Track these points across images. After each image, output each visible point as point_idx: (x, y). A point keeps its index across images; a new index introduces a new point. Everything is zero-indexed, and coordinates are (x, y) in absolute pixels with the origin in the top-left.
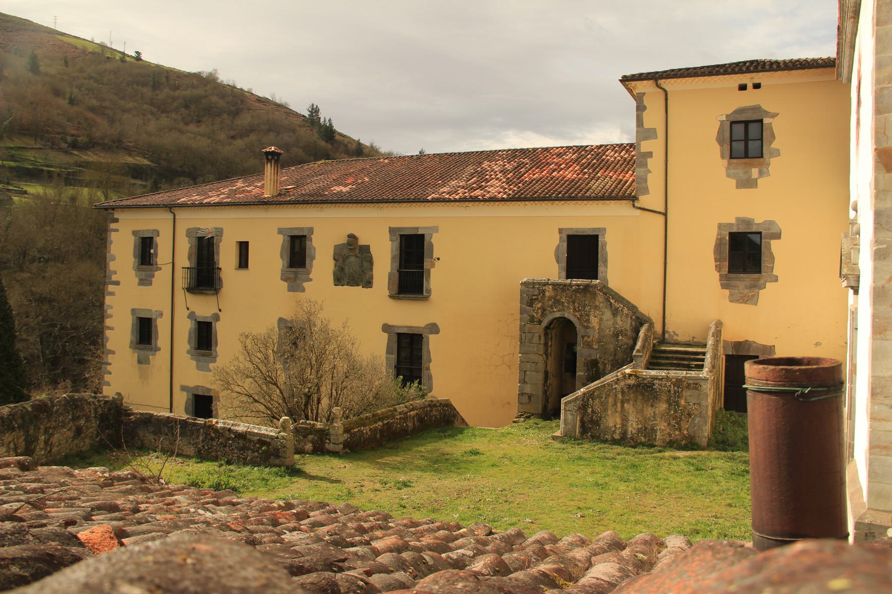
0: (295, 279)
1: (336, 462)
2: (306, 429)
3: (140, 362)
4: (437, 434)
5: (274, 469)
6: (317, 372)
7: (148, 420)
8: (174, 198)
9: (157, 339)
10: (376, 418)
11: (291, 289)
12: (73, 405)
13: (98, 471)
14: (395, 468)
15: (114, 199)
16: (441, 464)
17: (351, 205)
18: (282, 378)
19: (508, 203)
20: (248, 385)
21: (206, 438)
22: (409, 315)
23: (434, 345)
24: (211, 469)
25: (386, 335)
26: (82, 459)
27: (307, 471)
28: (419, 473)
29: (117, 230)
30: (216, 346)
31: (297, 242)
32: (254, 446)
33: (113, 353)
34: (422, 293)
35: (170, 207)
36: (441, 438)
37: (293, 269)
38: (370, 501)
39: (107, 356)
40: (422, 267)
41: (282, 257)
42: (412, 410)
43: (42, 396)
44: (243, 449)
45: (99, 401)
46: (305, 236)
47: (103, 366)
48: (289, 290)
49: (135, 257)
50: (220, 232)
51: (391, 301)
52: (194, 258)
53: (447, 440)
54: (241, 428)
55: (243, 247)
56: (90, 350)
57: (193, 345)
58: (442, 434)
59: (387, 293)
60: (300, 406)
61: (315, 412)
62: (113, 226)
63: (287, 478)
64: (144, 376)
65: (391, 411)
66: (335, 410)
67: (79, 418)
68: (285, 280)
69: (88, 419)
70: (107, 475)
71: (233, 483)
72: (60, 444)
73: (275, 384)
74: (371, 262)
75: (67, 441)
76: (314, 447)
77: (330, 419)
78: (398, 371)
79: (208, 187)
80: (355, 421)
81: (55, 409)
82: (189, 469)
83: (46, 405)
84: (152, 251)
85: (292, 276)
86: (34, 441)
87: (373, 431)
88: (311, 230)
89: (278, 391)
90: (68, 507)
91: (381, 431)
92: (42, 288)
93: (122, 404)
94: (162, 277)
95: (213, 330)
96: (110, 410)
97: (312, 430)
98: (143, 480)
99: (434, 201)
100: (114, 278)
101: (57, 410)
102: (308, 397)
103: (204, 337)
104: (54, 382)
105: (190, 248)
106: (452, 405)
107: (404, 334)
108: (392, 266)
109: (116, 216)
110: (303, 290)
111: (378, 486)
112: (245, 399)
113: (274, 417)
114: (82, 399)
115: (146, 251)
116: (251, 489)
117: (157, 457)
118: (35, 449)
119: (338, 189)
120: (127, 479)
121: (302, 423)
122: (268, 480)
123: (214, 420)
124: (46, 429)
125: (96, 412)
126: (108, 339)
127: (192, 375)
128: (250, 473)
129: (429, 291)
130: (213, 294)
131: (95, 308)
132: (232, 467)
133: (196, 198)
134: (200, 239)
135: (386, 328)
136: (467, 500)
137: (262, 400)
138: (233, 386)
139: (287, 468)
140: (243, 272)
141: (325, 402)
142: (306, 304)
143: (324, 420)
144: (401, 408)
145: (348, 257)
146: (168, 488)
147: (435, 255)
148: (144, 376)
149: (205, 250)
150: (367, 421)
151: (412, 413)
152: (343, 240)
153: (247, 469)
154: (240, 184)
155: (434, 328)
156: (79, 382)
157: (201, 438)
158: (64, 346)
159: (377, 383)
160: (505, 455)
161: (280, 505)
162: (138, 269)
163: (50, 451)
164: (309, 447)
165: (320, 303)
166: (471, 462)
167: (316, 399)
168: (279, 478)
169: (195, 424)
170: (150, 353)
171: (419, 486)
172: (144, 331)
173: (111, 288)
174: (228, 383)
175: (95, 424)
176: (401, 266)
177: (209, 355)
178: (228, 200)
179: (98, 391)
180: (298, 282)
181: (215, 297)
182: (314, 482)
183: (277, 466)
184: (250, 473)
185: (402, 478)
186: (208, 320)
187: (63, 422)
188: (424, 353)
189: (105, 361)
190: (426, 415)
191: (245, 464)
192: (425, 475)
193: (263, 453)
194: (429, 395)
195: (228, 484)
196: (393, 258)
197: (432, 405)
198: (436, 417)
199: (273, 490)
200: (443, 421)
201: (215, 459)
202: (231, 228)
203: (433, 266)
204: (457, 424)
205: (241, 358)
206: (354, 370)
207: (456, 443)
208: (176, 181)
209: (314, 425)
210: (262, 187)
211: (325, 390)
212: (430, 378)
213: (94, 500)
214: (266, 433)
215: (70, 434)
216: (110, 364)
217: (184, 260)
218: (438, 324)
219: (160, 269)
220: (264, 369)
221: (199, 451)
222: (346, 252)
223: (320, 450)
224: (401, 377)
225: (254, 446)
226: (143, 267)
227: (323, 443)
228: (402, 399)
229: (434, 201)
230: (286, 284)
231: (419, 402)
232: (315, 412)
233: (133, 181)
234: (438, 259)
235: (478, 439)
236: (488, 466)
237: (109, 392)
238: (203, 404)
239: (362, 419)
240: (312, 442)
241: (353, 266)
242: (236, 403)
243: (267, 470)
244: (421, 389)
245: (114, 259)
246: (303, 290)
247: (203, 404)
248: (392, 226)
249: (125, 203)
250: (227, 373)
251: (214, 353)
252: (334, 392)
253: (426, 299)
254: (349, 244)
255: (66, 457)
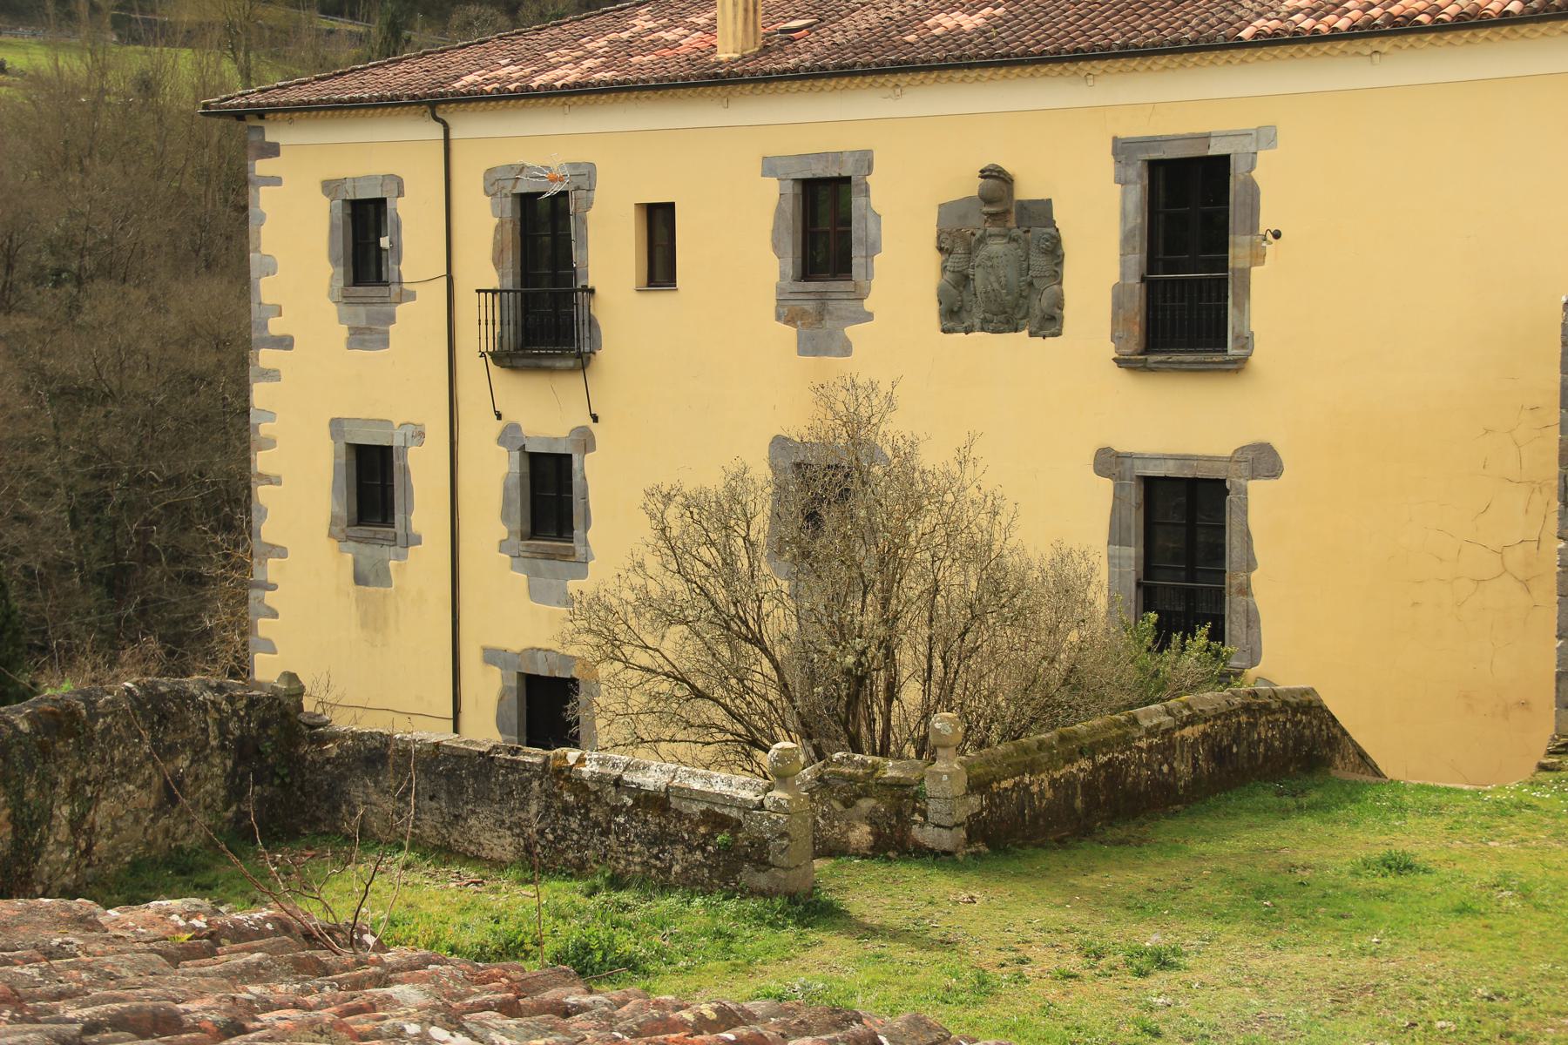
0: (821, 316)
1: (943, 884)
2: (852, 779)
3: (360, 579)
4: (1272, 799)
5: (752, 904)
6: (885, 603)
7: (375, 755)
8: (441, 75)
9: (408, 511)
10: (1072, 748)
11: (810, 346)
12: (157, 711)
13: (176, 913)
14: (1135, 907)
15: (273, 84)
16: (1276, 901)
17: (988, 73)
18: (779, 621)
19: (1524, 29)
20: (674, 644)
21: (548, 807)
22: (1182, 421)
23: (1262, 511)
24: (563, 900)
25: (1107, 485)
26: (182, 872)
27: (854, 911)
28: (1209, 927)
29: (276, 181)
30: (587, 527)
31: (824, 193)
32: (692, 832)
33: (282, 552)
34: (1221, 344)
35: (434, 104)
36: (1285, 813)
37: (812, 286)
38: (1047, 1009)
39: (263, 564)
40: (1223, 265)
41: (776, 248)
42: (1191, 721)
43: (60, 688)
44: (660, 839)
45: (231, 700)
46: (848, 180)
47: (253, 594)
48: (802, 351)
49: (334, 260)
50: (586, 175)
51: (1122, 377)
52: (511, 257)
53: (1306, 821)
54: (652, 778)
55: (659, 221)
56: (217, 547)
57: (517, 526)
58: (1290, 802)
59: (1110, 350)
60: (842, 707)
61: (879, 726)
62: (262, 167)
63: (789, 934)
64: (373, 622)
65: (1118, 725)
66: (943, 722)
67: (171, 751)
68: (790, 321)
69: (200, 753)
70: (200, 923)
71: (626, 944)
72: (117, 830)
73: (757, 641)
74: (1054, 250)
75: (137, 821)
76: (877, 835)
77: (925, 747)
78: (1148, 596)
79: (544, 35)
80: (1005, 756)
81: (99, 727)
82: (498, 902)
83: (73, 714)
84: (384, 242)
85: (810, 306)
86: (38, 823)
87: (1064, 788)
88: (865, 160)
89: (766, 665)
90: (23, 1020)
91: (1088, 787)
92: (73, 362)
93: (300, 708)
94: (417, 319)
95: (576, 479)
96: (264, 724)
97: (867, 785)
98: (309, 937)
99: (1265, 41)
100: (275, 327)
101: (108, 729)
102: (858, 680)
103: (549, 498)
104: (112, 642)
105: (499, 228)
106: (1322, 709)
107: (1166, 478)
108: (1123, 264)
109: (270, 137)
110: (846, 350)
111: (1073, 962)
112: (665, 686)
113: (754, 742)
114: (183, 698)
115: (365, 235)
116: (682, 964)
117: (407, 867)
118: (41, 844)
119: (946, 21)
120: (262, 934)
121: (840, 763)
122: (732, 937)
123: (573, 755)
124: (74, 783)
125: (223, 732)
126: (264, 513)
127: (519, 617)
128: (680, 913)
129: (1246, 341)
130: (571, 370)
131: (229, 424)
132: (625, 897)
133: (510, 72)
134: (527, 202)
135: (1108, 462)
136: (1366, 1022)
137: (719, 692)
138: (627, 650)
139: (792, 898)
140: (660, 300)
141: (912, 693)
142: (842, 395)
143: (910, 751)
144: (1152, 715)
145: (981, 240)
146: (380, 962)
147: (1266, 223)
148: (373, 622)
149: (543, 229)
150: (1043, 756)
151: (1188, 731)
152: (971, 186)
153: (672, 901)
154: (642, 21)
155: (1264, 461)
156: (184, 644)
157: (534, 808)
158: (144, 535)
159: (1074, 636)
160: (1506, 876)
161: (701, 1018)
162: (346, 300)
163: (88, 851)
164: (861, 834)
165: (885, 387)
166: (1384, 896)
167: (882, 685)
168: (765, 931)
169: (514, 766)
170: (388, 551)
171: (1203, 967)
172: (371, 484)
173: (266, 357)
174: (614, 641)
175: (220, 765)
176: (1152, 263)
177: (567, 556)
178: (608, 75)
179: (241, 669)
180: (828, 324)
181: (576, 381)
182: (874, 946)
183: (763, 894)
184: (680, 913)
185: (1153, 939)
186: (561, 450)
187: (124, 762)
188: (1233, 541)
189: (258, 577)
190: (1235, 740)
191: (665, 888)
192: (1227, 932)
193: (722, 856)
194: (1251, 673)
195: (612, 947)
196: (1126, 240)
197: (1256, 707)
198: (1269, 746)
199: (746, 968)
200: (1296, 753)
201: (578, 870)
202: (621, 160)
203: (1258, 257)
204: (1341, 771)
205: (653, 564)
206: (1000, 591)
207: (1336, 830)
208: (456, 20)
209: (875, 767)
210: (711, 28)
211: (908, 660)
212: (1252, 619)
213: (116, 999)
214: (725, 790)
215: (147, 799)
216: (274, 587)
217: (483, 265)
218: (1277, 446)
219: (412, 296)
220: (721, 596)
221: (528, 849)
222: (977, 224)
223: (894, 845)
224: (1153, 616)
225: (692, 832)
226: (361, 290)
227: (905, 823)
228: (1154, 688)
229: (1265, 41)
230: (790, 332)
231: (1211, 698)
232: (879, 726)
233: (326, 23)
234: (1277, 235)
235: (1412, 821)
236: (1444, 911)
237: (266, 670)
238: (547, 704)
239: (1026, 750)
240: (871, 820)
241: (999, 267)
242: (638, 700)
243: (732, 905)
244: (1217, 655)
245: (271, 269)
246: (846, 350)
247: (547, 704)
248: (1123, 134)
249: (294, 95)
250: (609, 609)
251: (580, 550)
252: (937, 662)
253: (1237, 366)
254: (986, 198)
255: (135, 867)
